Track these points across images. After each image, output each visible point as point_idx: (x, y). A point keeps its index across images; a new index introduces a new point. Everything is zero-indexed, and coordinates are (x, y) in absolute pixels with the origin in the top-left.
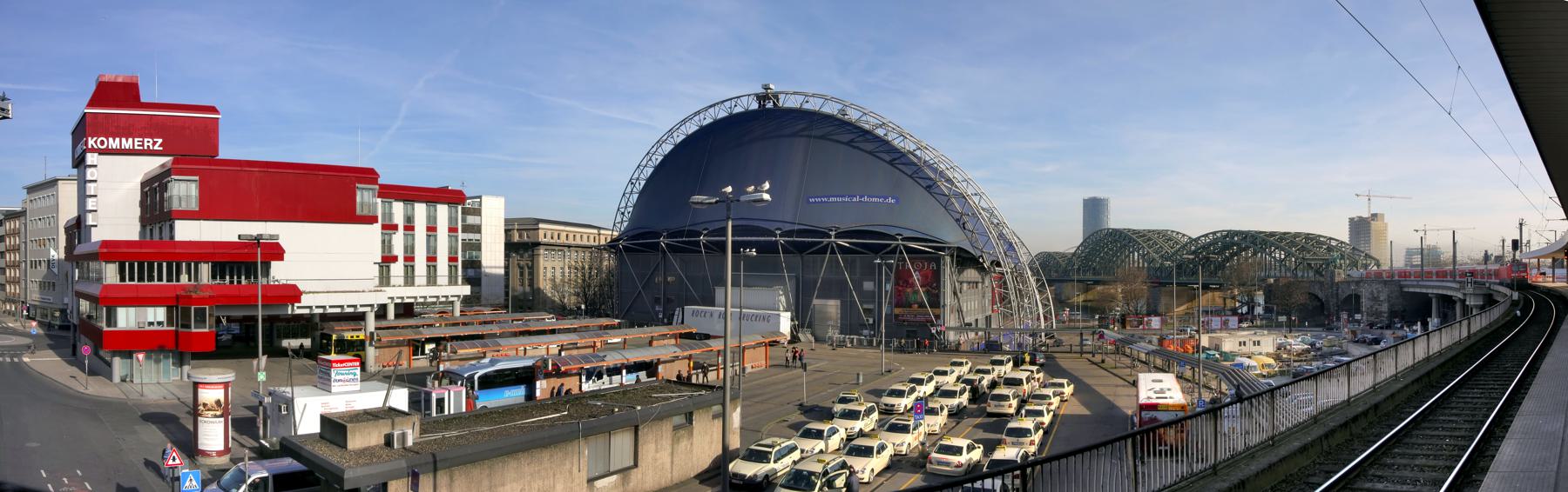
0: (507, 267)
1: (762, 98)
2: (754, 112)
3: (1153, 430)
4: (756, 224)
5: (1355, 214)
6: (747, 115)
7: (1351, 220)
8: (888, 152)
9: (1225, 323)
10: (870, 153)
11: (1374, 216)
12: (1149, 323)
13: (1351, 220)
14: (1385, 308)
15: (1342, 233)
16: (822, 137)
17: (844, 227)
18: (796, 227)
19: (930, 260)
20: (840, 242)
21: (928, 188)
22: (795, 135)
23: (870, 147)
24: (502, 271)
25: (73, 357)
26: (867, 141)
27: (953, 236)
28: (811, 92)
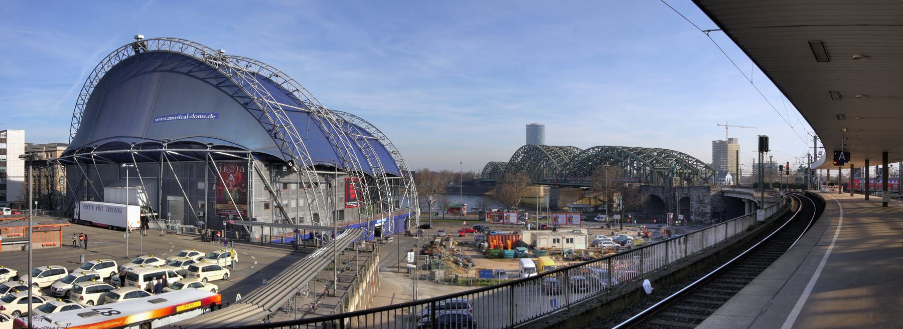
0: (27, 177)
1: (135, 46)
2: (133, 57)
3: (641, 249)
4: (123, 140)
5: (717, 139)
6: (130, 60)
7: (714, 142)
8: (215, 78)
9: (569, 220)
10: (202, 80)
11: (731, 140)
12: (508, 218)
13: (714, 142)
14: (708, 209)
15: (706, 156)
16: (171, 71)
17: (173, 140)
18: (143, 141)
19: (240, 164)
20: (170, 151)
21: (245, 105)
22: (154, 71)
23: (201, 75)
24: (23, 180)
25: (455, 214)
26: (201, 70)
27: (254, 141)
28: (165, 36)
